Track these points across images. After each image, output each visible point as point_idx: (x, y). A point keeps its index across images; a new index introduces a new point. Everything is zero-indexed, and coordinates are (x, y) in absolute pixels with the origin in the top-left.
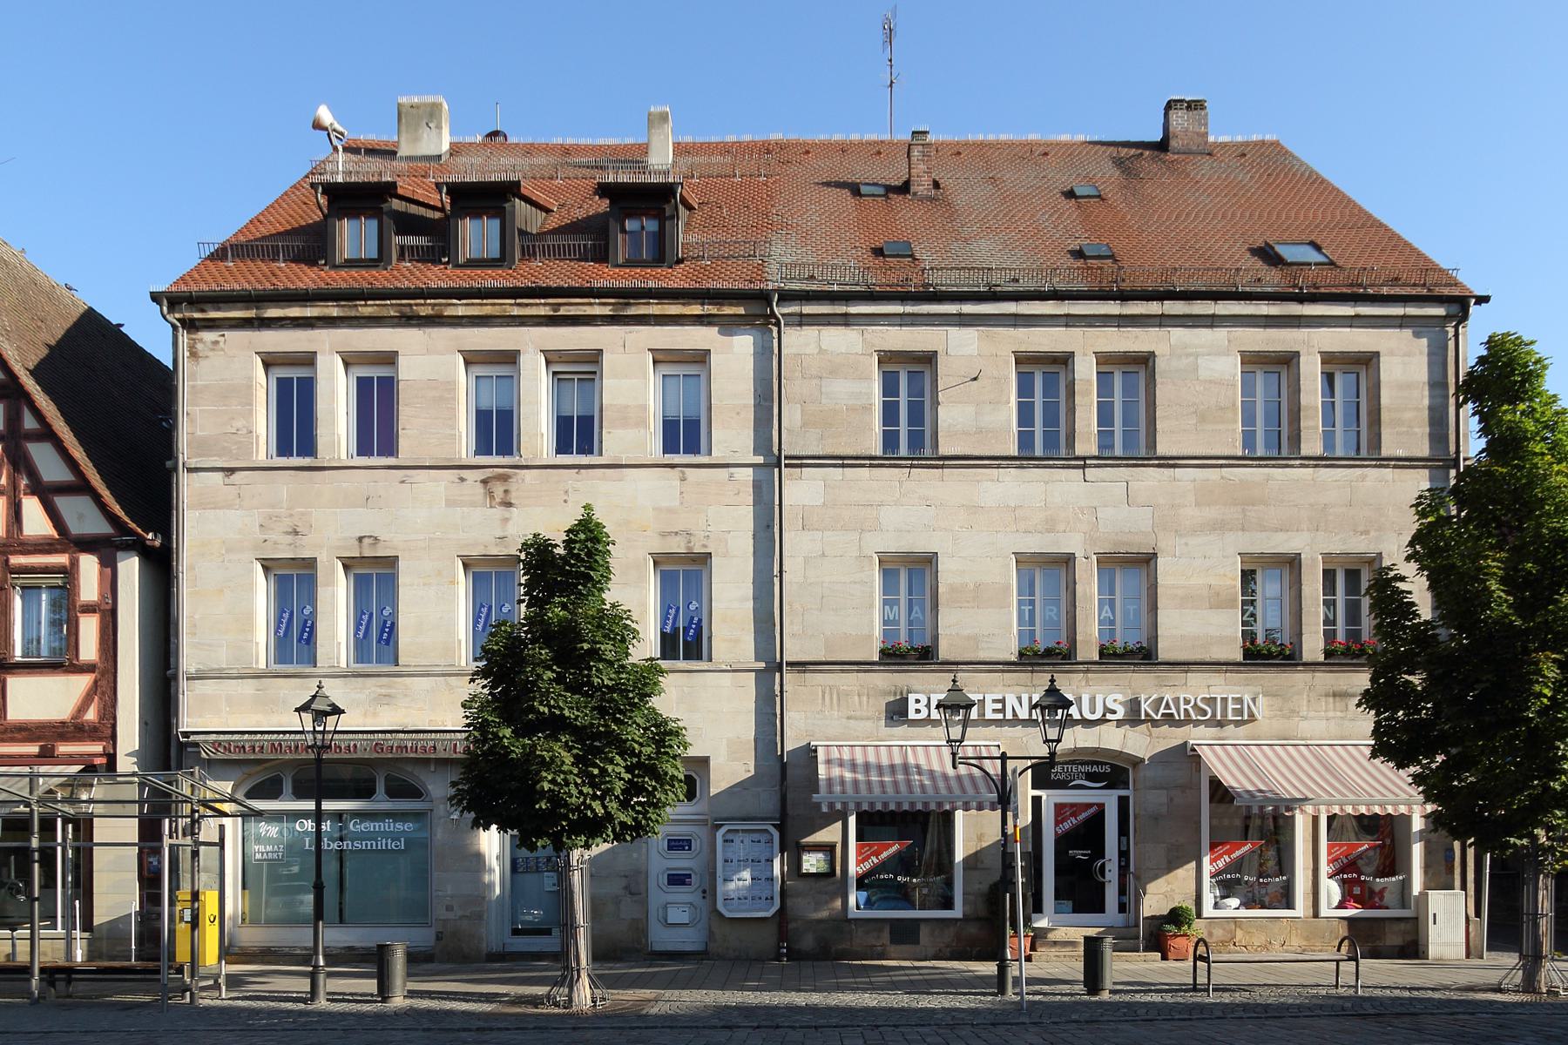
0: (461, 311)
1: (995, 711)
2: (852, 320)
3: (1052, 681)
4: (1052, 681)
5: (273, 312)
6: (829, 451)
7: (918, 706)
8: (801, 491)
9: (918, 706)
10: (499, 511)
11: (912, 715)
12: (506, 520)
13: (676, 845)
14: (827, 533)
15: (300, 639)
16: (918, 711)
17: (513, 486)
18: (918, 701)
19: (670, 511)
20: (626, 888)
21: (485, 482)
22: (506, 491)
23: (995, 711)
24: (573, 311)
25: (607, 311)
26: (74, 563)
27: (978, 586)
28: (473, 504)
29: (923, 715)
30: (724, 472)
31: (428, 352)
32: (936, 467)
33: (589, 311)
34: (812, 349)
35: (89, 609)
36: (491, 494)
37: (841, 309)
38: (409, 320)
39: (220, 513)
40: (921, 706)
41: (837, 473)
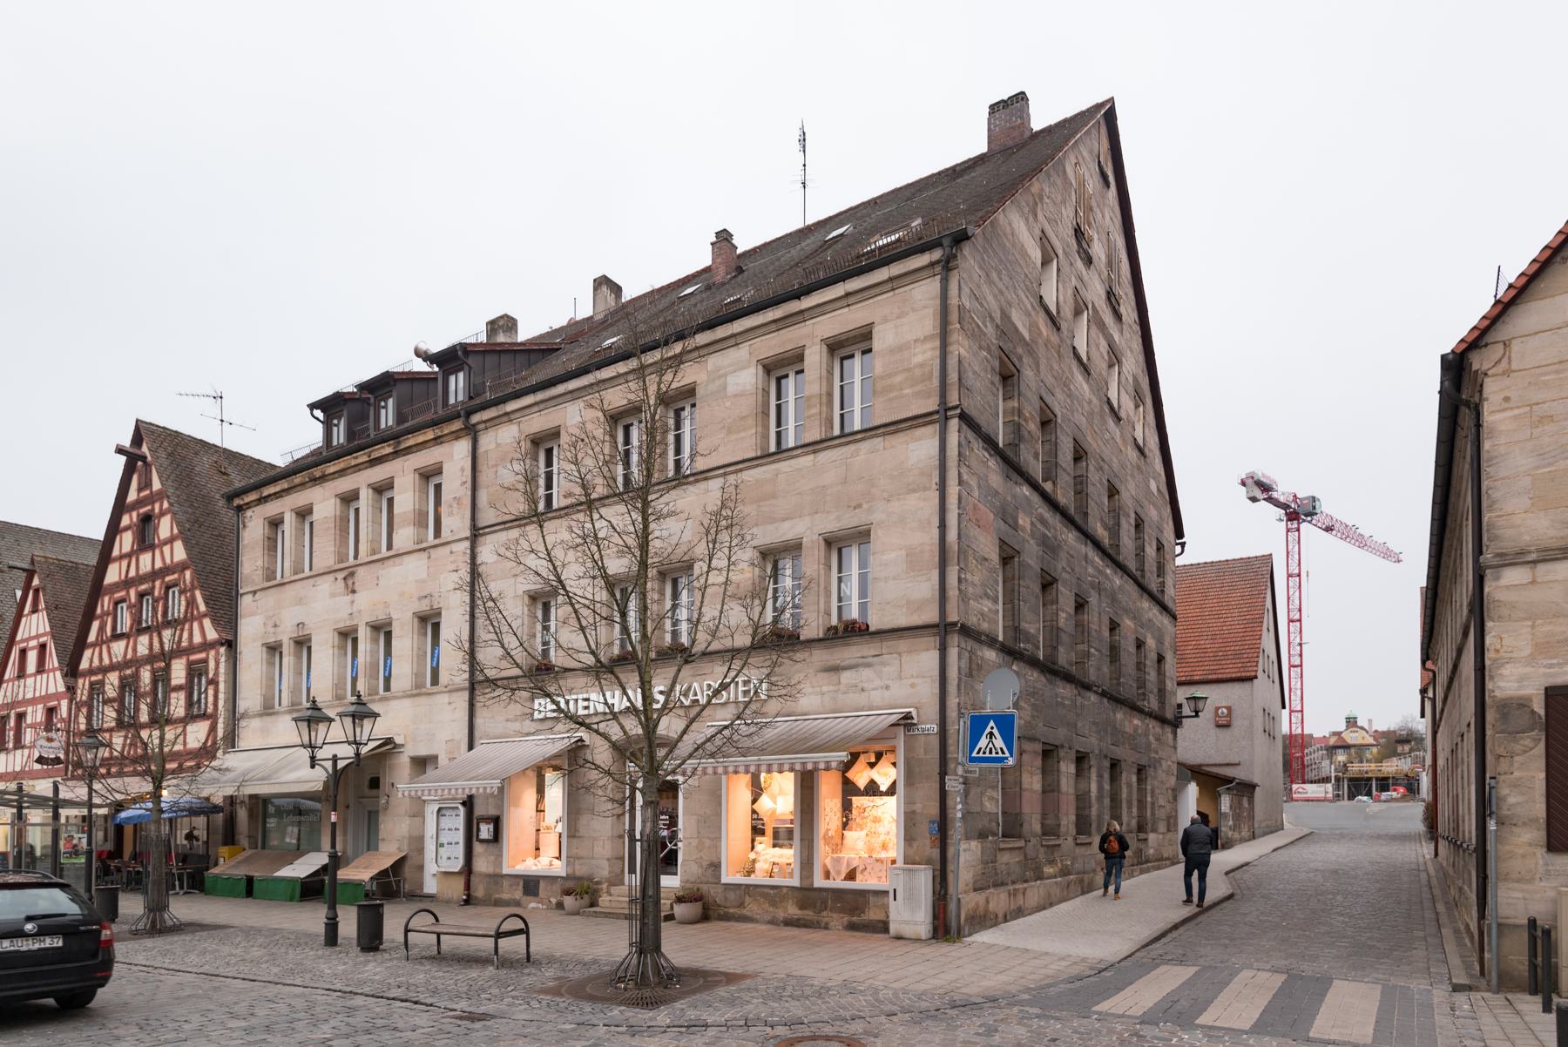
0: (332, 470)
19: (423, 581)
30: (447, 549)
34: (492, 446)
38: (317, 481)
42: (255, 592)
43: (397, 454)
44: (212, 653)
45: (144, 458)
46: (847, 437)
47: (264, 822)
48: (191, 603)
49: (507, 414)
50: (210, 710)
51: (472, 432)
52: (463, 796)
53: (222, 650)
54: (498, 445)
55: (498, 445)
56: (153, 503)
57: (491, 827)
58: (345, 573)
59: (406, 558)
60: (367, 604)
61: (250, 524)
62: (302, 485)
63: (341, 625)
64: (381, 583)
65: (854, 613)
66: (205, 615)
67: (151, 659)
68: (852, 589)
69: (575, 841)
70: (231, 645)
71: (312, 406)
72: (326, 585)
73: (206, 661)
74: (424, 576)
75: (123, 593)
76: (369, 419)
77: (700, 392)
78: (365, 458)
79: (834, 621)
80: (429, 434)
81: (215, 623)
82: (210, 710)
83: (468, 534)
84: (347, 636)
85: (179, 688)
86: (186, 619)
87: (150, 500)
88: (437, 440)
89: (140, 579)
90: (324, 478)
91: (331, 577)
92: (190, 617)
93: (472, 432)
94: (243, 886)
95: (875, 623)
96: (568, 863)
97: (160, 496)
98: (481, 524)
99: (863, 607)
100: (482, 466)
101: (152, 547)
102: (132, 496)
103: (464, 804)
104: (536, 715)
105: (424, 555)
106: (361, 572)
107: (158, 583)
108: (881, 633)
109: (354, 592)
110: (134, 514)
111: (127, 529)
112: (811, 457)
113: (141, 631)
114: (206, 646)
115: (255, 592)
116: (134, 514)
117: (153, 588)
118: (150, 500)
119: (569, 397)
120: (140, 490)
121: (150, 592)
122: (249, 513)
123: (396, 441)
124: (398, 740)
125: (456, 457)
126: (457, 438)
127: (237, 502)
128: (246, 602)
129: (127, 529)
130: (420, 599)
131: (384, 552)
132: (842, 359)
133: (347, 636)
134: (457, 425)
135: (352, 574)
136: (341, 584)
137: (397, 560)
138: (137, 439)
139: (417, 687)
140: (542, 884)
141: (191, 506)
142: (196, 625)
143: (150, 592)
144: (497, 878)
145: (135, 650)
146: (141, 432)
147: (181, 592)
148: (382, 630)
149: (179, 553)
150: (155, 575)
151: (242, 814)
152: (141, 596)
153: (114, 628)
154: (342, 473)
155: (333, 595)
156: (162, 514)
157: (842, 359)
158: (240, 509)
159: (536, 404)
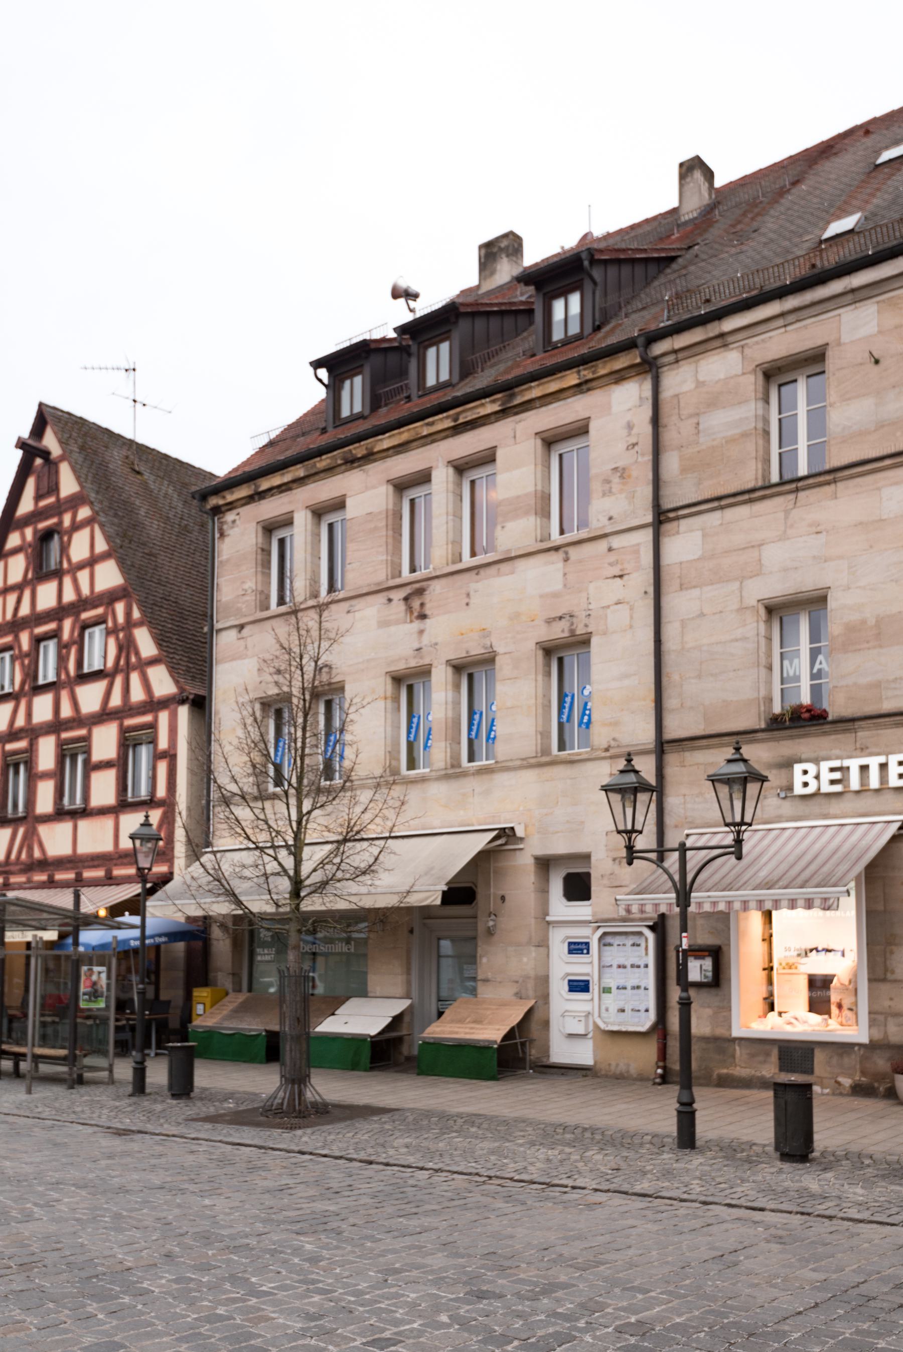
0: (386, 444)
1: (833, 782)
2: (730, 339)
3: (147, 817)
4: (147, 817)
5: (265, 484)
6: (707, 495)
7: (806, 778)
8: (322, 642)
9: (806, 778)
10: (417, 625)
11: (798, 790)
12: (421, 632)
13: (578, 948)
14: (706, 589)
15: (580, 723)
16: (806, 784)
17: (427, 597)
18: (805, 772)
19: (555, 595)
20: (516, 994)
21: (406, 599)
22: (422, 605)
23: (833, 782)
24: (470, 416)
25: (496, 407)
26: (156, 719)
27: (879, 621)
28: (397, 622)
29: (811, 789)
30: (603, 545)
31: (367, 488)
32: (828, 483)
33: (483, 411)
34: (689, 386)
35: (45, 775)
36: (410, 609)
37: (713, 329)
38: (352, 462)
39: (234, 663)
40: (809, 778)
41: (714, 519)
42: (241, 627)
43: (504, 413)
44: (164, 717)
45: (45, 454)
46: (792, 484)
47: (252, 955)
48: (127, 646)
49: (722, 335)
50: (161, 792)
51: (650, 368)
52: (651, 913)
53: (183, 712)
54: (699, 384)
55: (699, 384)
56: (60, 514)
57: (708, 963)
58: (403, 593)
59: (521, 564)
60: (449, 630)
61: (233, 534)
62: (330, 470)
63: (400, 666)
64: (473, 601)
65: (805, 699)
66: (153, 662)
67: (56, 726)
68: (802, 666)
69: (884, 988)
70: (201, 705)
71: (317, 364)
72: (370, 611)
73: (153, 726)
74: (558, 586)
75: (52, 626)
76: (396, 388)
77: (832, 363)
78: (449, 423)
79: (777, 709)
80: (571, 378)
81: (173, 671)
82: (161, 792)
83: (649, 518)
84: (408, 683)
85: (106, 765)
86: (116, 669)
87: (58, 509)
88: (582, 387)
89: (38, 618)
90: (370, 457)
91: (381, 598)
92: (127, 662)
93: (650, 368)
94: (261, 1048)
95: (835, 707)
96: (872, 1023)
97: (75, 502)
98: (667, 504)
99: (816, 690)
100: (669, 417)
101: (58, 574)
102: (26, 505)
103: (652, 928)
104: (798, 790)
105: (559, 556)
106: (436, 588)
107: (67, 624)
108: (848, 723)
109: (423, 617)
110: (29, 532)
111: (15, 551)
112: (717, 514)
113: (39, 689)
114: (153, 705)
115: (241, 627)
116: (29, 532)
117: (60, 629)
118: (58, 509)
119: (850, 297)
120: (38, 497)
121: (55, 634)
122: (230, 517)
123: (451, 409)
124: (520, 832)
125: (615, 408)
126: (618, 382)
127: (214, 501)
128: (225, 642)
129: (15, 551)
130: (549, 621)
131: (467, 560)
132: (780, 386)
133: (408, 683)
134: (633, 358)
135: (420, 592)
136: (399, 607)
137: (504, 567)
138: (39, 428)
139: (453, 766)
140: (819, 1057)
141: (116, 515)
142: (135, 677)
143: (55, 634)
144: (724, 1044)
145: (29, 715)
146: (44, 418)
147: (109, 633)
148: (471, 671)
149: (109, 576)
150: (59, 612)
151: (221, 944)
152: (38, 641)
153: (80, 663)
154: (401, 448)
155: (384, 624)
156: (76, 527)
157: (780, 386)
158: (217, 511)
159: (782, 315)
